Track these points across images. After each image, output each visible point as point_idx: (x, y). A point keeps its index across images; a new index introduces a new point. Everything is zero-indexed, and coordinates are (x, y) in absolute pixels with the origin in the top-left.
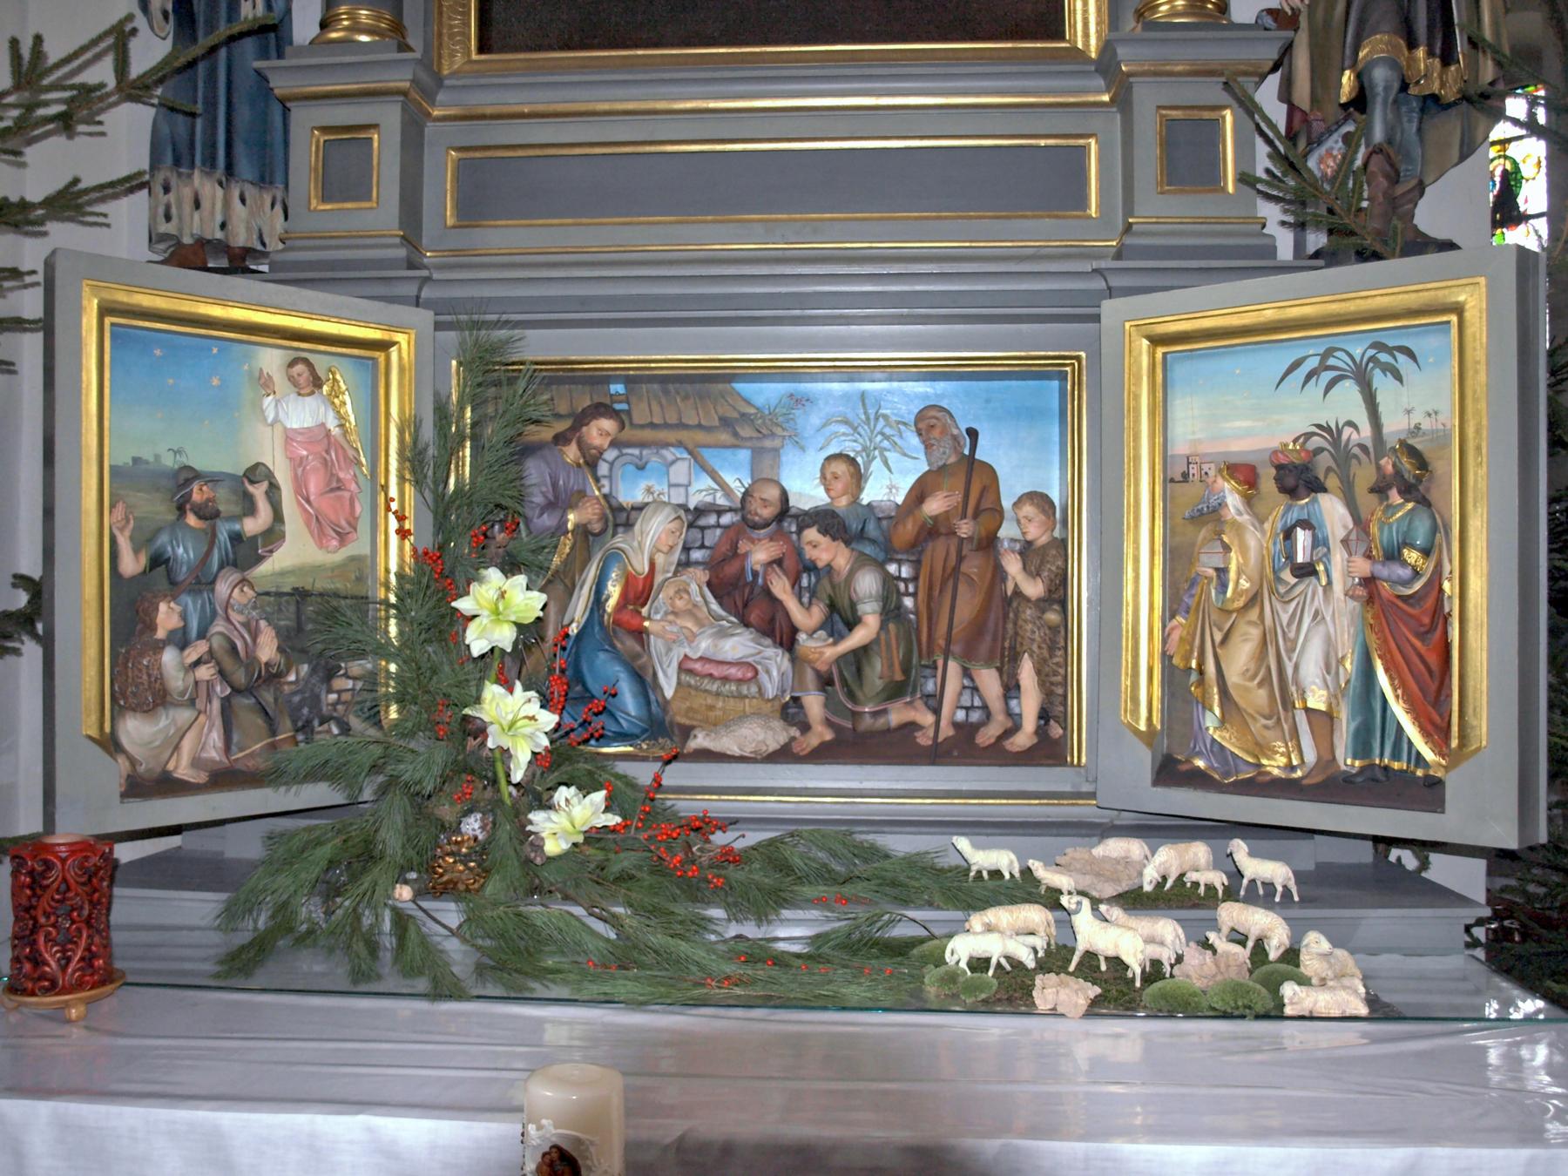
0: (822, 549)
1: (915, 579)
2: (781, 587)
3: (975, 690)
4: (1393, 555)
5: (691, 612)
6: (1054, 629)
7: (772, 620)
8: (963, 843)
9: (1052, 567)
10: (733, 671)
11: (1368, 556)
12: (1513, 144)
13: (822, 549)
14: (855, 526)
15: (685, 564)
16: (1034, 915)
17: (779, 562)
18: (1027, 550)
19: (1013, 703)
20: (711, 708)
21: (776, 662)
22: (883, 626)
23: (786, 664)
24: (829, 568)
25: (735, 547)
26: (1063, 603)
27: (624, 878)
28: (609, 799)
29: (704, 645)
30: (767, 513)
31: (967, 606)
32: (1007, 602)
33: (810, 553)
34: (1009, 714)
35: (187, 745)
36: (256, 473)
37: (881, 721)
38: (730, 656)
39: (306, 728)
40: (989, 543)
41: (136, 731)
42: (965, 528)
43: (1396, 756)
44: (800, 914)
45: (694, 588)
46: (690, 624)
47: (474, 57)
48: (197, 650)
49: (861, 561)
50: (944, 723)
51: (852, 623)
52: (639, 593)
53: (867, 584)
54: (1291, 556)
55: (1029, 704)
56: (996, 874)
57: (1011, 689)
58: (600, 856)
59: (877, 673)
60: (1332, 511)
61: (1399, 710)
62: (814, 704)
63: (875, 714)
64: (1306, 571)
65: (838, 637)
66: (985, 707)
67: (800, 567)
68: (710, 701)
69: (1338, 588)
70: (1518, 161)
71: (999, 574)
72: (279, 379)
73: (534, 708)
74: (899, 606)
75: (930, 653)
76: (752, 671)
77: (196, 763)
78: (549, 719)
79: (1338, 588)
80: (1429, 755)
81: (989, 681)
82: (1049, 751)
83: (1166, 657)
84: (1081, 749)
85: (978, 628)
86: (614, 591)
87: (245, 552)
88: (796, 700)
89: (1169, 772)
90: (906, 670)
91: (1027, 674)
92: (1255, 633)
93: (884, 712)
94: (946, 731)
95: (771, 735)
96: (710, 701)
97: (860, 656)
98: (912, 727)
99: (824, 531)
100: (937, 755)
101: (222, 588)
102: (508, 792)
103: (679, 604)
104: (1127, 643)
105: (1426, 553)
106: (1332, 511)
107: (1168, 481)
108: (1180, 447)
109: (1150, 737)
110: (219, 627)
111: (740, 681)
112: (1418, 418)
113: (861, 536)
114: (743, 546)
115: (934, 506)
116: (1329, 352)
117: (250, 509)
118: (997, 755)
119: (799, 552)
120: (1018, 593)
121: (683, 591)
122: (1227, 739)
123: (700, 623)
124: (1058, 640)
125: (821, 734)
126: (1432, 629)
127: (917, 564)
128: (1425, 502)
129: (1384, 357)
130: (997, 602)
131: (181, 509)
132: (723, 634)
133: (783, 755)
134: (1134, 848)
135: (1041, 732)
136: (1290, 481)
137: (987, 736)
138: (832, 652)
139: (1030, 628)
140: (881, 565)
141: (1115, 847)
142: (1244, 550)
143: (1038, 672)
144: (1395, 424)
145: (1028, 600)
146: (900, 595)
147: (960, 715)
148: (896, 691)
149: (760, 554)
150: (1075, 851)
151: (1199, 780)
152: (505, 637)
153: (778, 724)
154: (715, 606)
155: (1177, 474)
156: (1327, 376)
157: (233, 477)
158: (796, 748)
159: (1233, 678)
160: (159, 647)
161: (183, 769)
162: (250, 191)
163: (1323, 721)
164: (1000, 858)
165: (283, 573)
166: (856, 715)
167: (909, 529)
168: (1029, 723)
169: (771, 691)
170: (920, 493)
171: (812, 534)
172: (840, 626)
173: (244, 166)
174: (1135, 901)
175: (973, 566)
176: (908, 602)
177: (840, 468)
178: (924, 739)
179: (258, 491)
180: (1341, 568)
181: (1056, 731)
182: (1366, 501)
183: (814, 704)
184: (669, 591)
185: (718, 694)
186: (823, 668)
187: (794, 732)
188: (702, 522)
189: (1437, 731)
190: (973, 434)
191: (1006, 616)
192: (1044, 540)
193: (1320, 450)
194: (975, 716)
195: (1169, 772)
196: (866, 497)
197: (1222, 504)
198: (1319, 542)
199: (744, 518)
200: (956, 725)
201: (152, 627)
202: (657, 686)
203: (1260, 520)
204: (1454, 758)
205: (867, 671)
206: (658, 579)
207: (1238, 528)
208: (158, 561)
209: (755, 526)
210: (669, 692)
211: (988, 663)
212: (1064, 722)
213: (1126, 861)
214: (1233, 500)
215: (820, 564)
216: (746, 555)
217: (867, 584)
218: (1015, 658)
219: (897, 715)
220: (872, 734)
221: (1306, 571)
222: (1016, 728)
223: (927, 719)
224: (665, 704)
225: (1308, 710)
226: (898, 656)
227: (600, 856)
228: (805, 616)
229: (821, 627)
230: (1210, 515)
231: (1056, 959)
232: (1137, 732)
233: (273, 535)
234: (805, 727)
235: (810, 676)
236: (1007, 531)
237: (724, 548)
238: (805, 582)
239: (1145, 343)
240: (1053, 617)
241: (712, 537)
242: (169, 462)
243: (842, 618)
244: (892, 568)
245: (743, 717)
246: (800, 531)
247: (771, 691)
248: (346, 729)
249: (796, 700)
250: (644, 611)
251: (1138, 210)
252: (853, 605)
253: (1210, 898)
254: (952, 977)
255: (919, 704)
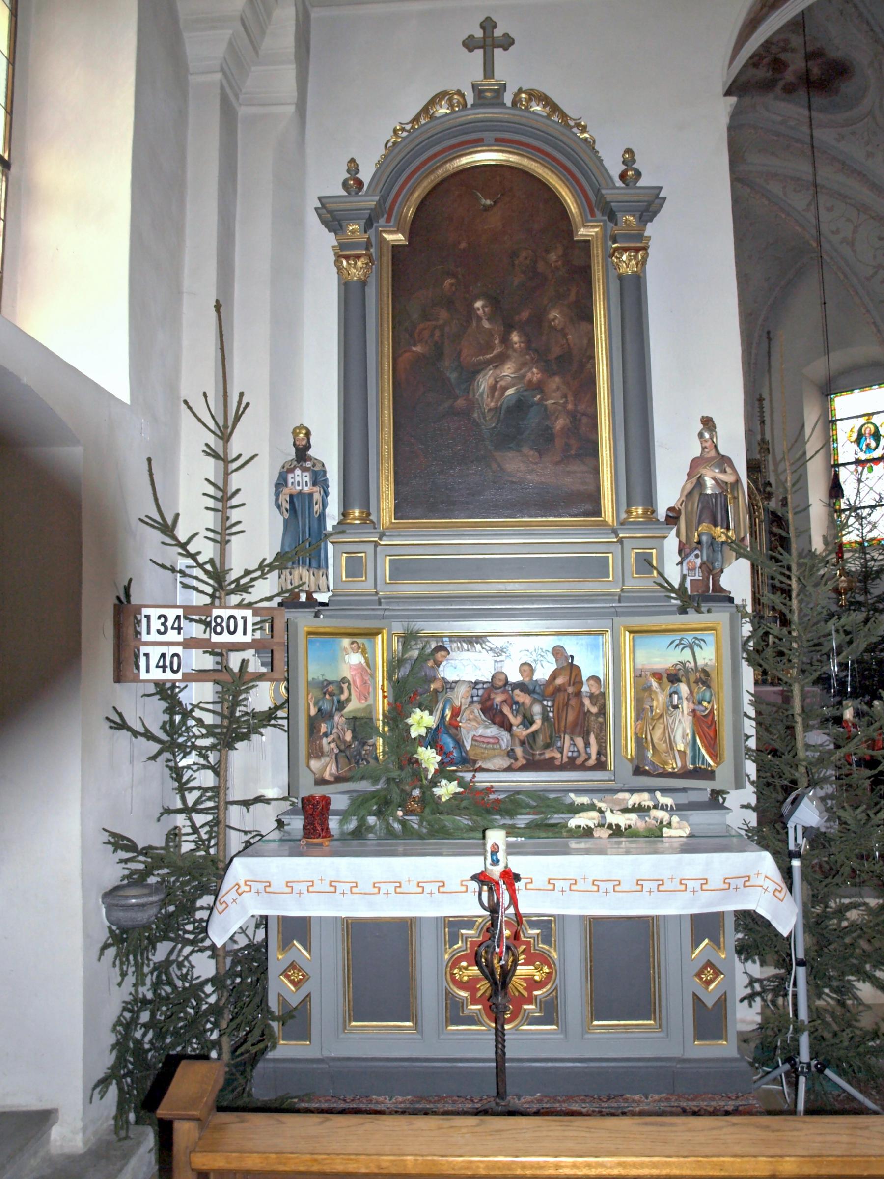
0: (521, 697)
1: (553, 706)
2: (506, 710)
3: (575, 745)
4: (700, 703)
5: (475, 719)
6: (601, 724)
7: (503, 722)
8: (572, 795)
9: (601, 702)
10: (491, 740)
11: (693, 703)
12: (875, 416)
13: (521, 697)
14: (531, 687)
15: (472, 702)
16: (594, 814)
17: (505, 701)
18: (592, 696)
19: (588, 749)
20: (483, 753)
21: (505, 736)
22: (543, 724)
23: (509, 738)
24: (523, 703)
25: (489, 696)
26: (604, 714)
27: (466, 808)
28: (458, 783)
29: (481, 731)
30: (501, 684)
31: (571, 716)
32: (585, 714)
33: (517, 698)
34: (587, 753)
35: (328, 769)
36: (344, 680)
37: (542, 757)
38: (489, 735)
39: (357, 763)
40: (578, 694)
41: (315, 764)
42: (570, 690)
43: (703, 764)
44: (523, 817)
45: (476, 711)
46: (474, 723)
47: (394, 521)
48: (332, 737)
49: (535, 701)
50: (564, 757)
51: (532, 722)
52: (456, 713)
53: (537, 709)
54: (671, 702)
55: (594, 749)
56: (583, 804)
57: (587, 744)
58: (456, 802)
59: (540, 740)
60: (684, 688)
61: (703, 751)
62: (519, 751)
63: (540, 754)
64: (676, 707)
65: (527, 728)
66: (578, 751)
67: (512, 702)
68: (483, 750)
69: (685, 712)
70: (878, 425)
71: (582, 704)
72: (349, 650)
73: (434, 755)
74: (548, 716)
75: (559, 732)
76: (497, 740)
77: (331, 774)
78: (439, 758)
79: (685, 712)
80: (712, 763)
81: (580, 742)
82: (601, 766)
83: (636, 734)
84: (611, 766)
85: (575, 724)
86: (448, 713)
87: (341, 705)
88: (512, 750)
89: (638, 771)
90: (551, 738)
91: (592, 739)
92: (662, 726)
93: (544, 753)
94: (565, 760)
95: (505, 762)
96: (483, 750)
97: (534, 735)
98: (553, 759)
99: (521, 691)
100: (562, 768)
101: (336, 718)
102: (425, 782)
103: (471, 716)
104: (623, 729)
105: (709, 703)
106: (684, 688)
107: (635, 677)
108: (639, 666)
109: (631, 760)
110: (335, 731)
111: (493, 744)
112: (707, 661)
113: (534, 691)
114: (492, 696)
115: (559, 681)
116: (681, 639)
117: (342, 692)
118: (583, 767)
119: (512, 697)
120: (589, 711)
121: (472, 712)
122: (654, 760)
123: (478, 723)
124: (603, 727)
125: (522, 762)
126: (711, 726)
127: (553, 701)
128: (709, 687)
129: (697, 642)
130: (581, 715)
131: (325, 694)
132: (487, 727)
133: (509, 769)
134: (626, 795)
135: (598, 759)
136: (671, 679)
137: (579, 761)
138: (525, 733)
139: (594, 724)
140: (541, 702)
141: (621, 796)
142: (658, 700)
143: (596, 739)
144: (701, 662)
145: (592, 713)
146: (548, 712)
147: (570, 754)
148: (547, 746)
149: (498, 698)
150: (608, 797)
151: (647, 773)
152: (423, 732)
153: (507, 758)
154: (483, 717)
155: (638, 674)
156: (681, 646)
157: (336, 682)
158: (513, 766)
159: (655, 740)
160: (321, 738)
161: (327, 776)
162: (316, 571)
163: (683, 754)
164: (585, 800)
165: (350, 712)
166: (533, 755)
167: (551, 689)
168: (594, 756)
169: (504, 747)
170: (554, 676)
171: (517, 692)
172: (527, 723)
173: (314, 564)
174: (625, 810)
175: (573, 702)
176: (551, 715)
177: (526, 668)
178: (557, 763)
179: (345, 686)
180: (686, 706)
181: (603, 759)
182: (693, 685)
183: (519, 751)
184: (467, 712)
185: (486, 748)
186: (522, 738)
187: (512, 761)
188: (478, 687)
189: (713, 756)
190: (572, 657)
191: (585, 719)
192: (597, 692)
193: (679, 669)
194: (575, 754)
195: (638, 771)
196: (535, 678)
197: (651, 685)
198: (680, 698)
199: (492, 686)
200: (568, 757)
201: (320, 731)
202: (464, 746)
203: (663, 690)
204: (718, 764)
205: (537, 739)
206: (463, 708)
207: (656, 693)
208: (320, 710)
209: (497, 689)
210: (468, 748)
211: (579, 735)
212: (606, 756)
213: (624, 800)
214: (655, 684)
215: (520, 702)
216: (493, 699)
217: (537, 709)
218: (588, 734)
219: (548, 755)
220: (540, 761)
221: (676, 707)
222: (589, 758)
223: (558, 755)
224: (466, 752)
225: (679, 751)
226: (548, 734)
227: (456, 802)
228: (515, 720)
229: (521, 724)
230: (649, 688)
231: (601, 825)
232: (627, 758)
233: (348, 700)
234: (516, 759)
235: (517, 742)
236: (585, 689)
237: (486, 696)
238: (514, 708)
239: (627, 633)
240: (601, 720)
241: (481, 692)
242: (321, 678)
243: (528, 721)
244: (545, 703)
245: (494, 756)
246: (513, 690)
247: (504, 747)
248: (368, 762)
249: (512, 750)
250: (458, 719)
251: (626, 583)
252: (532, 716)
253: (649, 809)
254: (570, 830)
255: (555, 750)
